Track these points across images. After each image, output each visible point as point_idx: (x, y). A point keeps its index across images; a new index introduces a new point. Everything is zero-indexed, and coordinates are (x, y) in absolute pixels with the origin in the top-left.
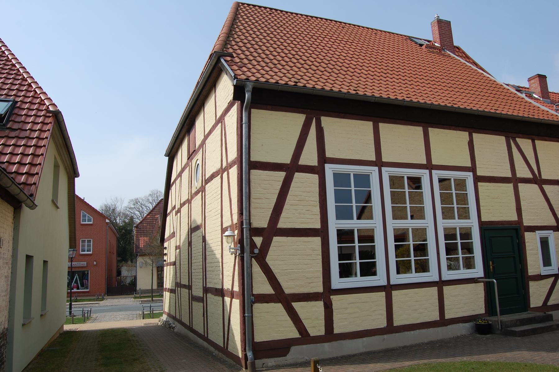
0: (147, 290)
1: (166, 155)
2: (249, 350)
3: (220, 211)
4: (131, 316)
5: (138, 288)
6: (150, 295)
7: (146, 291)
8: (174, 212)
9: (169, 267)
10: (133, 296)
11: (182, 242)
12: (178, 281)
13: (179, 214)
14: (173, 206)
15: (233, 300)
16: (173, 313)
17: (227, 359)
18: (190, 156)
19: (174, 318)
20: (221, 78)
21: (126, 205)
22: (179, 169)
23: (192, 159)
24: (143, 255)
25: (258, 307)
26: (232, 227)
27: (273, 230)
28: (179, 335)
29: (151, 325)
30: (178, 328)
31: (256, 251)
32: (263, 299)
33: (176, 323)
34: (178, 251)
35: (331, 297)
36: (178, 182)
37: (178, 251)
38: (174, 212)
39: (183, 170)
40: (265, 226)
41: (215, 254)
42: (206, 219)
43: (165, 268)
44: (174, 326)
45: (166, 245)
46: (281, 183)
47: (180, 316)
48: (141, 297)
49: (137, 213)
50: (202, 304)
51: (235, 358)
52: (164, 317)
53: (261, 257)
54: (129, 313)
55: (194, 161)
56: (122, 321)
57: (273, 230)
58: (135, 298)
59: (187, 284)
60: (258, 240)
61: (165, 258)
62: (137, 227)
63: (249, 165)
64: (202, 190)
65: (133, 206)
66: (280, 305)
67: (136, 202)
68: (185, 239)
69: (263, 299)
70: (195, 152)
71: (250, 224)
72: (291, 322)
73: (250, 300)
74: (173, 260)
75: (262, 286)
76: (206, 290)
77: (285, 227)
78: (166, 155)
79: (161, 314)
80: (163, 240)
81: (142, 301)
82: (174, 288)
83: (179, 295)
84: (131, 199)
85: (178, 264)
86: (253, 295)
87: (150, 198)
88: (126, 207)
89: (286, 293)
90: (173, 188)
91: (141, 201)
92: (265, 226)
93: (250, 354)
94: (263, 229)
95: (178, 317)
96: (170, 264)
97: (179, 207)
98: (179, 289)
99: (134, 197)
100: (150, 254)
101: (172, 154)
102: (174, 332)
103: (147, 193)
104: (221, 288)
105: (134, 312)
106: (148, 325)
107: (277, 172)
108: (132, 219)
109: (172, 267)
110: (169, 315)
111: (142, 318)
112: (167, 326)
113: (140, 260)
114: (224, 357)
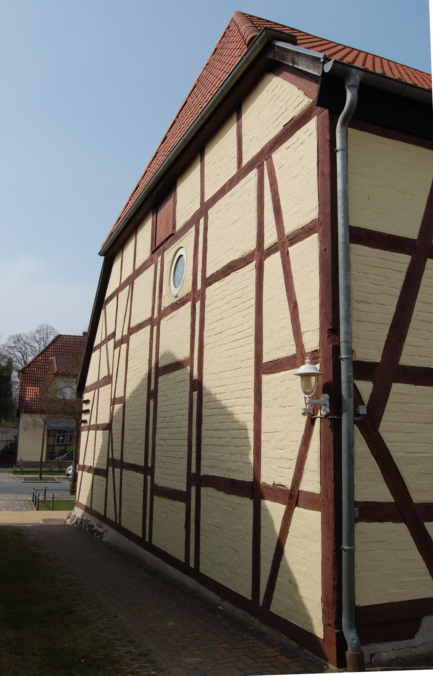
0: (286, 512)
1: (100, 254)
2: (350, 627)
3: (129, 362)
4: (16, 502)
5: (19, 459)
6: (38, 470)
7: (31, 464)
8: (111, 343)
9: (92, 432)
10: (12, 470)
11: (129, 391)
12: (117, 456)
13: (124, 346)
14: (110, 332)
15: (298, 510)
16: (99, 508)
17: (265, 628)
18: (157, 248)
19: (103, 518)
20: (260, 87)
21: (4, 343)
22: (128, 272)
23: (165, 250)
24: (31, 412)
25: (366, 531)
26: (314, 357)
27: (389, 371)
28: (114, 549)
29: (55, 523)
30: (110, 535)
31: (363, 410)
32: (372, 512)
33: (106, 527)
34: (118, 407)
35: (202, 475)
36: (124, 294)
37: (118, 407)
38: (111, 343)
39: (137, 273)
40: (378, 359)
41: (231, 414)
42: (206, 348)
43: (84, 434)
44: (101, 530)
45: (87, 396)
46: (403, 276)
47: (119, 513)
48: (23, 473)
49: (18, 354)
50: (183, 505)
51: (306, 637)
52: (78, 512)
53: (370, 425)
54: (11, 496)
55: (169, 254)
56: (5, 512)
57: (389, 371)
58: (15, 472)
59: (142, 463)
60: (366, 388)
61: (85, 417)
62: (22, 372)
63: (340, 234)
64: (197, 297)
65: (13, 345)
66: (403, 527)
67: (18, 339)
68: (140, 386)
69: (372, 512)
70: (173, 237)
71: (350, 351)
72: (422, 564)
73: (343, 516)
74: (104, 419)
75: (371, 487)
76: (197, 480)
77: (412, 365)
78: (100, 254)
79: (71, 505)
80: (81, 388)
81: (25, 479)
82: (105, 468)
83: (117, 480)
84: (11, 334)
85: (117, 427)
86: (356, 504)
87: (38, 336)
88: (4, 346)
89: (415, 501)
90: (110, 307)
91: (24, 338)
92: (378, 359)
93: (351, 637)
94: (374, 365)
95: (111, 515)
96: (97, 427)
97: (125, 333)
98: (117, 470)
99: (16, 332)
100: (42, 412)
101: (112, 251)
102: (103, 542)
103: (34, 328)
104: (249, 478)
105: (19, 497)
106: (51, 523)
107: (395, 254)
108: (10, 362)
109: (100, 433)
110: (88, 510)
111: (35, 510)
112: (81, 526)
113: (25, 418)
114: (256, 622)
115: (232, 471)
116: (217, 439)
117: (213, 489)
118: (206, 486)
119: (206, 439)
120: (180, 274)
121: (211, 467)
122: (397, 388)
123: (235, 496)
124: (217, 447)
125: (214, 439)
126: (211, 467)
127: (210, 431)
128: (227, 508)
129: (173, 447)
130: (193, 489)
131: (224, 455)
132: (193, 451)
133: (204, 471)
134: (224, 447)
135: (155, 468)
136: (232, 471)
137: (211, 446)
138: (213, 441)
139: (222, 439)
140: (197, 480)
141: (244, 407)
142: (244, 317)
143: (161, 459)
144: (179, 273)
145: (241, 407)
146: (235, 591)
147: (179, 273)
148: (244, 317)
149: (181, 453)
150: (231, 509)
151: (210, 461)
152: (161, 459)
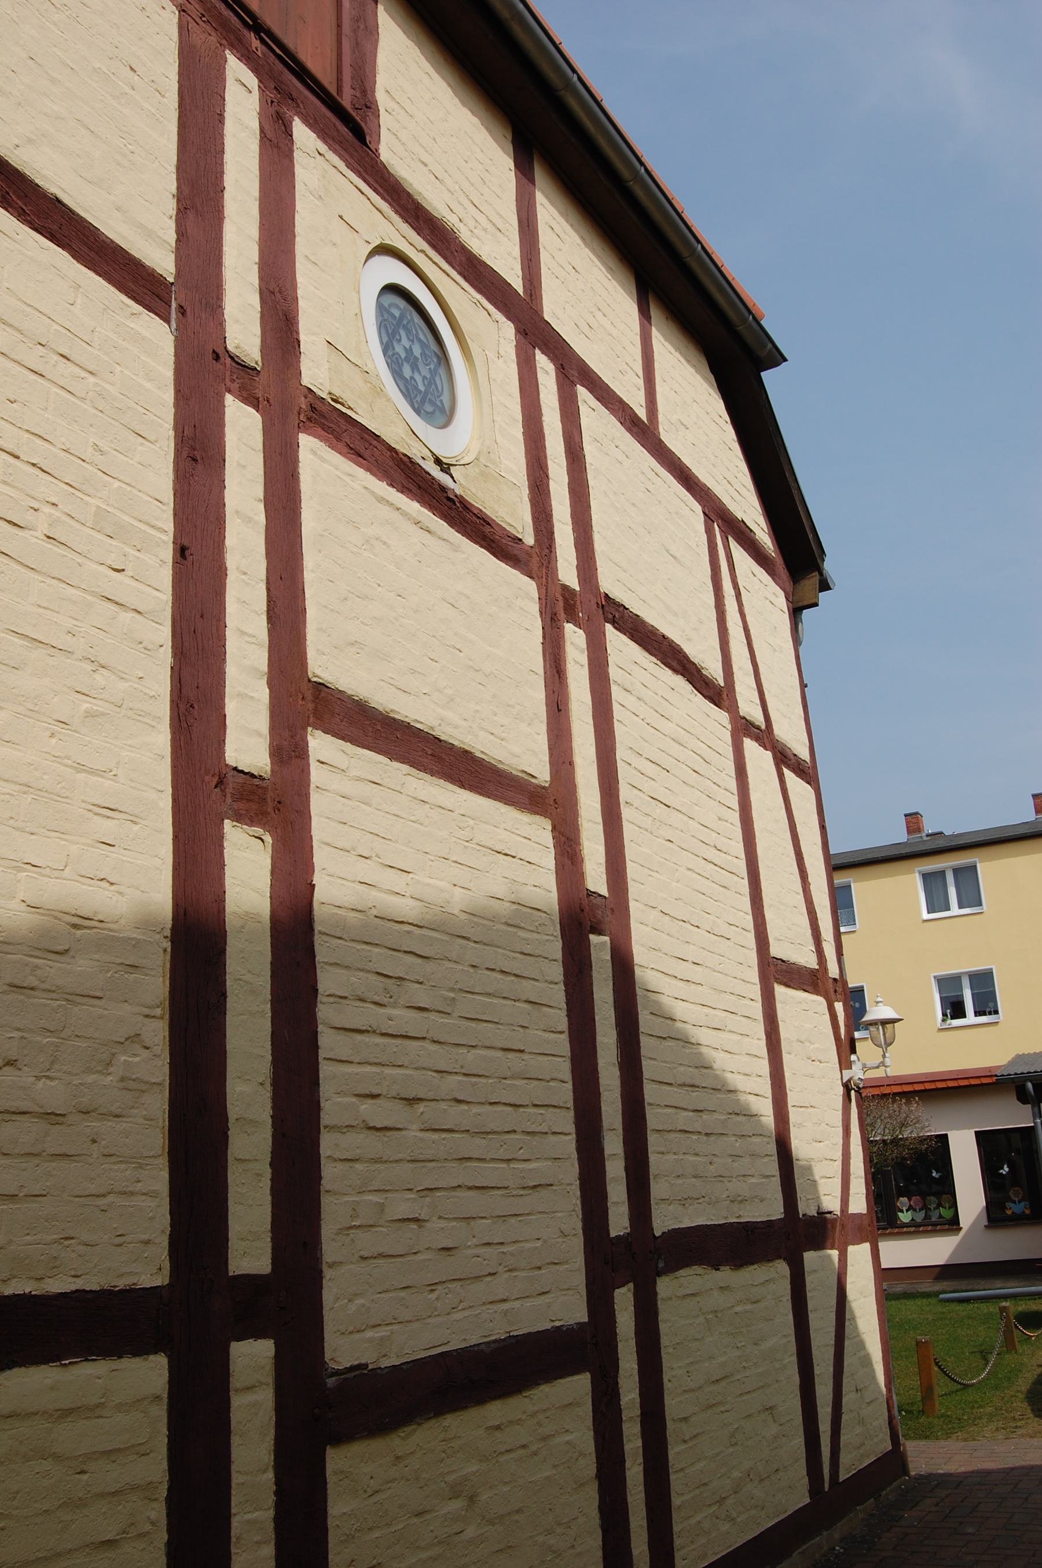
20: (597, 244)
35: (658, 1233)
115: (741, 1202)
116: (691, 1114)
117: (697, 1269)
118: (675, 1265)
119: (660, 1110)
120: (409, 351)
121: (683, 1202)
122: (148, 1268)
123: (755, 1266)
124: (695, 1137)
125: (686, 1114)
126: (683, 1202)
127: (668, 1088)
128: (738, 1309)
129: (478, 1140)
130: (624, 1299)
131: (715, 1159)
132: (607, 1151)
133: (664, 1220)
134: (713, 1138)
135: (328, 1273)
136: (741, 1202)
137: (678, 1135)
138: (683, 1119)
139: (705, 1116)
140: (629, 1258)
141: (746, 1040)
142: (720, 819)
143: (381, 1207)
144: (417, 351)
145: (740, 1037)
146: (779, 1519)
147: (417, 351)
148: (720, 819)
149: (533, 1165)
150: (749, 1307)
151: (680, 1181)
152: (381, 1207)
